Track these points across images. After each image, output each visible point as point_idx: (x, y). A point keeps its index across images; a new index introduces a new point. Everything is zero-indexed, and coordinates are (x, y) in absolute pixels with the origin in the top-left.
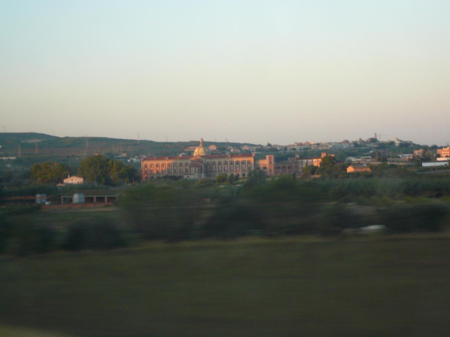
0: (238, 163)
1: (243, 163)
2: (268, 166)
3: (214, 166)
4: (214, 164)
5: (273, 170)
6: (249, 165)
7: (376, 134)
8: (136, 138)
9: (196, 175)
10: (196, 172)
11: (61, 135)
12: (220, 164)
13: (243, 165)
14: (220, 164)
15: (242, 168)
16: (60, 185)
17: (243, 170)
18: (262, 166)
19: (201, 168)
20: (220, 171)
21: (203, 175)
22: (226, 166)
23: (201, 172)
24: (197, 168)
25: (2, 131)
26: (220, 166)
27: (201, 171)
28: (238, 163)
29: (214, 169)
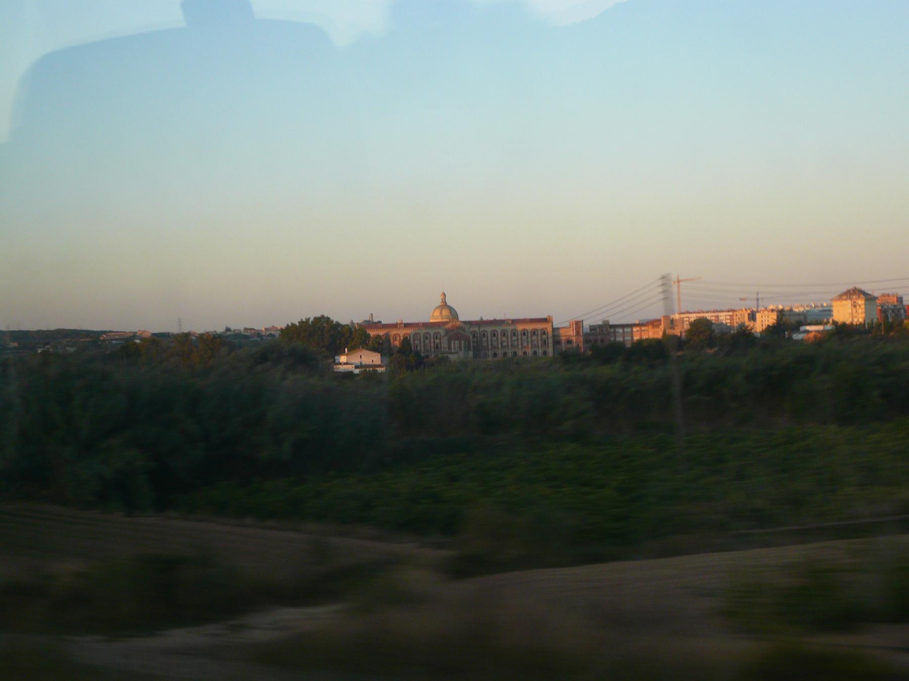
0: (524, 334)
1: (534, 332)
2: (574, 339)
3: (484, 339)
4: (484, 335)
5: (581, 345)
6: (544, 337)
7: (444, 295)
8: (78, 328)
9: (462, 354)
10: (460, 349)
11: (52, 328)
12: (494, 335)
13: (534, 338)
14: (494, 335)
15: (532, 342)
16: (797, 336)
17: (533, 346)
18: (563, 338)
19: (469, 343)
20: (505, 347)
21: (471, 354)
22: (504, 339)
23: (469, 349)
24: (463, 342)
25: (3, 328)
26: (494, 338)
27: (468, 348)
28: (524, 333)
29: (485, 344)
